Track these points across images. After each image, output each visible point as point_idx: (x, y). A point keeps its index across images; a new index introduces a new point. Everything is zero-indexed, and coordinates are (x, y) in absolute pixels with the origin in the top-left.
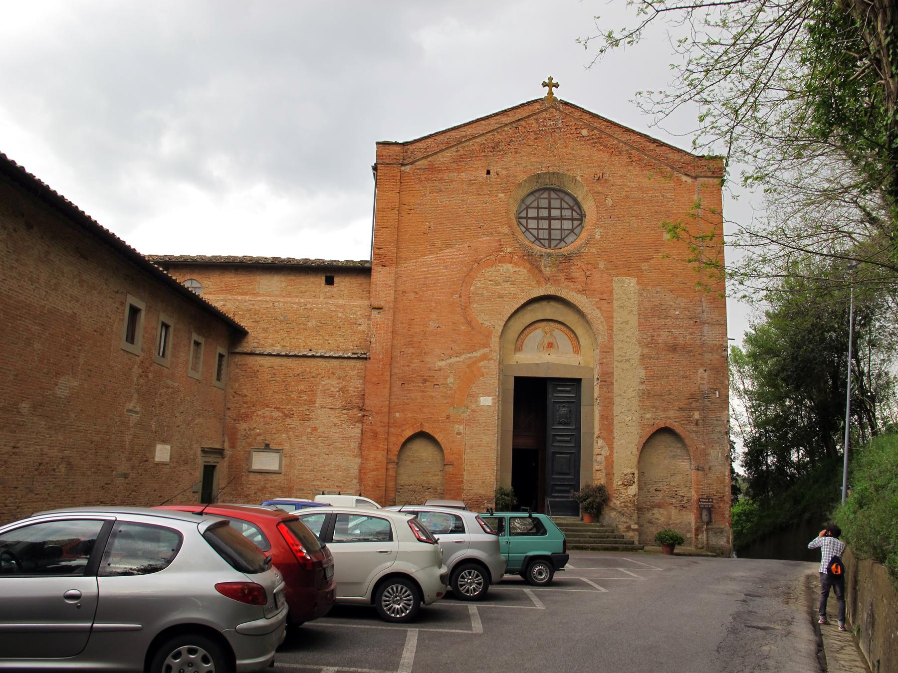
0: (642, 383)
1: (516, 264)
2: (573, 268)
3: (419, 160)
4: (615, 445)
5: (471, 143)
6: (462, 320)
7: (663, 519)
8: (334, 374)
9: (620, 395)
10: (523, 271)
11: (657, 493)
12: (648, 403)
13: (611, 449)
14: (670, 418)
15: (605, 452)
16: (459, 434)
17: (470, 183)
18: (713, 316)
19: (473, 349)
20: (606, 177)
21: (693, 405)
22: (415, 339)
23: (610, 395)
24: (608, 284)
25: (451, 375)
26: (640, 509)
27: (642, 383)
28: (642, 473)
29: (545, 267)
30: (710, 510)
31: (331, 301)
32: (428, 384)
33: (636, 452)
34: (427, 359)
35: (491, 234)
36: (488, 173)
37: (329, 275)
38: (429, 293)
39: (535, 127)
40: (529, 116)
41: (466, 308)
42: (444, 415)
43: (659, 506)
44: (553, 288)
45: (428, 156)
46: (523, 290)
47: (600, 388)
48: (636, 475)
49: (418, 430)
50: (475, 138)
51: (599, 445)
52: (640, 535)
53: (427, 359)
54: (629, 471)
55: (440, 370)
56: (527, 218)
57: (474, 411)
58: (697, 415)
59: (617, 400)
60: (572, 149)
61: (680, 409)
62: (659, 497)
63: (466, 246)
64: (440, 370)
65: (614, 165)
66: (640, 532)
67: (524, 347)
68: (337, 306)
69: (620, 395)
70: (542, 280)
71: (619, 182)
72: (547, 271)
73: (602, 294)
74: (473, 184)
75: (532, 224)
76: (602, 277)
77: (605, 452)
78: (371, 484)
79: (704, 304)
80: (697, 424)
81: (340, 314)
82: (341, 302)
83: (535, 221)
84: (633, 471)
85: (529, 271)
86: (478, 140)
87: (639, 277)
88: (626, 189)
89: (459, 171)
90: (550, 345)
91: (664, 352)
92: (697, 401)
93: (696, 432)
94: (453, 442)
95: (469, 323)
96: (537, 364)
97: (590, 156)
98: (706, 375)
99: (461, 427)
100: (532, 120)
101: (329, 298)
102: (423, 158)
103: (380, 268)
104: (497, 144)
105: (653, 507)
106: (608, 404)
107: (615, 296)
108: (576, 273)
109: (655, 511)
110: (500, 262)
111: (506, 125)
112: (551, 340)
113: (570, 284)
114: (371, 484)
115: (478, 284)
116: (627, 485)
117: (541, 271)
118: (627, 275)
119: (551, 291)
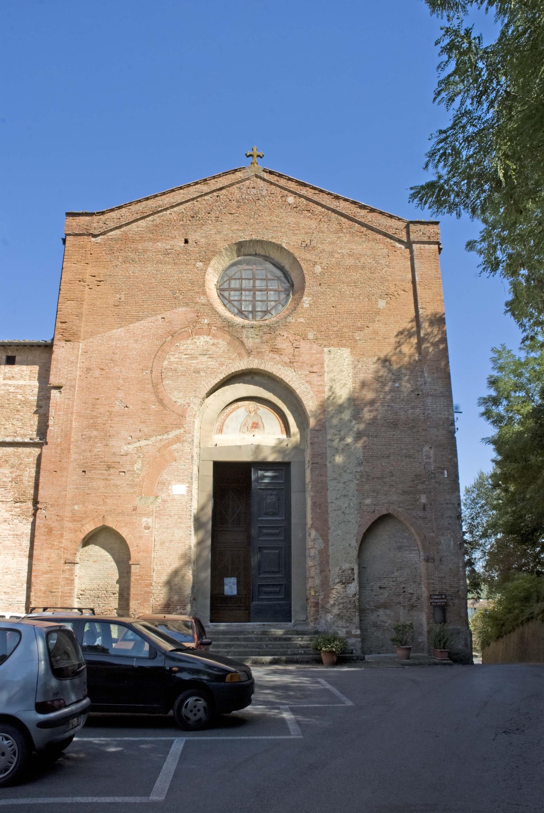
0: (360, 464)
1: (214, 336)
2: (279, 339)
3: (111, 230)
4: (330, 537)
5: (168, 212)
6: (153, 398)
7: (389, 622)
8: (7, 461)
9: (335, 479)
10: (222, 343)
11: (382, 591)
12: (367, 487)
13: (326, 541)
14: (391, 500)
15: (320, 544)
16: (147, 528)
17: (166, 253)
18: (435, 387)
19: (166, 430)
20: (314, 244)
21: (420, 487)
22: (100, 421)
23: (323, 478)
24: (318, 356)
25: (140, 461)
26: (362, 611)
27: (360, 464)
28: (362, 568)
29: (248, 337)
30: (443, 609)
31: (10, 382)
32: (112, 471)
33: (355, 544)
34: (112, 442)
35: (187, 305)
36: (186, 241)
37: (10, 354)
38: (117, 369)
39: (237, 195)
40: (232, 185)
41: (157, 384)
42: (130, 506)
43: (385, 606)
44: (256, 361)
45: (120, 227)
46: (222, 364)
47: (312, 471)
48: (356, 571)
49: (99, 525)
50: (172, 207)
51: (313, 541)
52: (363, 641)
53: (112, 442)
54: (346, 566)
55: (126, 455)
56: (230, 289)
57: (164, 501)
58: (423, 499)
59: (331, 484)
60: (277, 216)
61: (404, 492)
62: (384, 596)
63: (159, 317)
64: (126, 455)
65: (323, 232)
66: (363, 638)
67: (224, 429)
68: (18, 387)
69: (335, 479)
70: (243, 352)
71: (328, 248)
72: (249, 343)
73: (312, 367)
74: (168, 254)
75: (234, 296)
76: (311, 348)
77: (320, 544)
78: (43, 588)
79: (426, 375)
80: (424, 508)
81: (19, 397)
82: (21, 382)
83: (237, 293)
84: (351, 565)
85: (229, 344)
86: (175, 209)
87: (353, 348)
88: (336, 256)
89: (155, 241)
90: (255, 426)
91: (383, 429)
92: (423, 483)
93: (424, 518)
94: (141, 537)
95: (161, 401)
96: (240, 447)
97: (297, 224)
98: (432, 452)
99: (150, 520)
100: (234, 189)
101: (9, 379)
102: (116, 228)
103: (63, 343)
104: (197, 213)
105: (378, 607)
106: (321, 489)
107: (326, 369)
108: (283, 344)
109: (381, 612)
110: (196, 334)
111: (207, 194)
112: (255, 420)
113: (276, 356)
114: (43, 588)
115: (172, 359)
116: (345, 583)
117: (242, 343)
118: (340, 345)
119: (254, 363)
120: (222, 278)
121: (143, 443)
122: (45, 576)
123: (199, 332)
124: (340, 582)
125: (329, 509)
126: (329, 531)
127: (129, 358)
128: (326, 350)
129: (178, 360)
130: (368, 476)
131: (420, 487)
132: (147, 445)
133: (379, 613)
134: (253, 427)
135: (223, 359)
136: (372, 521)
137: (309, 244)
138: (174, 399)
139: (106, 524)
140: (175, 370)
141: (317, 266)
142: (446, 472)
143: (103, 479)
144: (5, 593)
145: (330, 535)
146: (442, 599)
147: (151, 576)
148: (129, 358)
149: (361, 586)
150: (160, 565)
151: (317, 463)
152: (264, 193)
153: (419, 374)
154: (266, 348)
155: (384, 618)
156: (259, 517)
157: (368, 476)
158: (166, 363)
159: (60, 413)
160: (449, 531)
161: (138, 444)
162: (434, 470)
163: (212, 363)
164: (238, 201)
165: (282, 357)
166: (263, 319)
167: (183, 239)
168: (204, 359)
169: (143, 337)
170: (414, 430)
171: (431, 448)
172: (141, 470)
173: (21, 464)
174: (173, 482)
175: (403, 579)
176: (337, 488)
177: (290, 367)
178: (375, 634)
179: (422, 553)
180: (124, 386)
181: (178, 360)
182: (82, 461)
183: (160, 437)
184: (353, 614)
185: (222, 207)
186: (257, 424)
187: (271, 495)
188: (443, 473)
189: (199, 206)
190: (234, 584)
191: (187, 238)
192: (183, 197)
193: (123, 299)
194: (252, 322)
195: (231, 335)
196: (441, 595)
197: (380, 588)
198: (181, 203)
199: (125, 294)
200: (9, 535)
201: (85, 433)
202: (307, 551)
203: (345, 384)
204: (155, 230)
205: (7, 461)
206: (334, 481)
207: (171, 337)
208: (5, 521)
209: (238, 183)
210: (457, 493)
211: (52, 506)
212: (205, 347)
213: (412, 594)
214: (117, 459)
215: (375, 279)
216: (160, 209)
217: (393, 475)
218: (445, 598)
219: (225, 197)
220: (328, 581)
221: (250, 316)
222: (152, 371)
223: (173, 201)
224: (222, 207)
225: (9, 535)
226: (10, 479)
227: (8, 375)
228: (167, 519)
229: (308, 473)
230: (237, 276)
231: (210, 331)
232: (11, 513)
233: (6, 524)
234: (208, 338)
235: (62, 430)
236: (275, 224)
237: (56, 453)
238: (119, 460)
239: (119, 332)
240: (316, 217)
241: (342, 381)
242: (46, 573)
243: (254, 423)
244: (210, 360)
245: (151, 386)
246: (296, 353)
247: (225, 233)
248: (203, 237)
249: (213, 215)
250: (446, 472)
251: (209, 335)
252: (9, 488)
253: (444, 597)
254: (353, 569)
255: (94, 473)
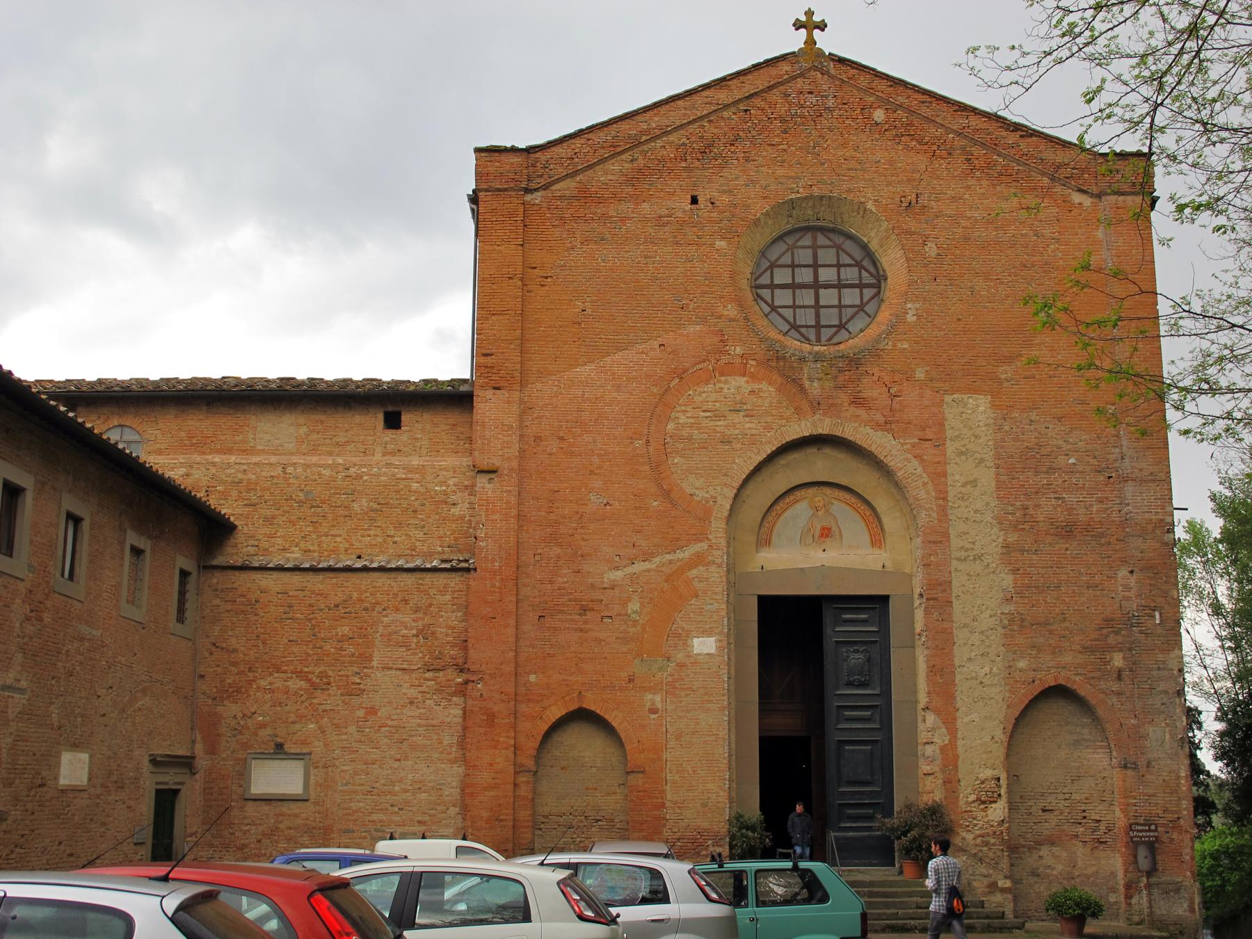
1: (753, 377)
2: (865, 380)
4: (959, 724)
7: (1060, 867)
8: (406, 601)
9: (966, 626)
13: (953, 732)
15: (941, 738)
16: (653, 711)
17: (660, 222)
19: (675, 544)
21: (1112, 640)
23: (946, 625)
26: (1013, 849)
27: (1008, 600)
28: (1014, 778)
31: (395, 460)
32: (589, 615)
35: (704, 320)
36: (694, 200)
37: (390, 409)
38: (587, 438)
42: (624, 675)
43: (1051, 841)
44: (827, 421)
45: (576, 173)
46: (768, 427)
47: (927, 612)
48: (1003, 782)
50: (666, 133)
52: (1016, 899)
54: (989, 773)
56: (772, 286)
57: (681, 666)
58: (1118, 661)
59: (960, 635)
60: (856, 148)
63: (656, 344)
65: (938, 178)
66: (1016, 894)
69: (966, 626)
70: (805, 406)
72: (814, 388)
74: (664, 225)
77: (941, 738)
79: (1125, 443)
80: (1119, 678)
81: (415, 486)
84: (996, 773)
85: (779, 390)
86: (672, 138)
88: (964, 223)
90: (826, 533)
91: (1049, 539)
93: (1119, 694)
94: (643, 727)
95: (666, 494)
96: (802, 570)
97: (891, 163)
98: (1132, 581)
99: (658, 698)
100: (775, 96)
101: (393, 454)
105: (1039, 843)
106: (943, 642)
107: (949, 433)
108: (870, 390)
109: (1045, 851)
110: (722, 374)
111: (726, 107)
113: (862, 412)
114: (485, 814)
116: (986, 801)
117: (802, 389)
119: (824, 426)
120: (758, 265)
121: (639, 567)
122: (487, 793)
123: (727, 370)
124: (978, 799)
125: (958, 677)
126: (958, 714)
127: (607, 418)
128: (948, 398)
129: (693, 421)
130: (1023, 620)
131: (1112, 640)
132: (648, 571)
133: (1041, 853)
134: (822, 535)
135: (769, 419)
136: (1031, 697)
137: (914, 201)
138: (689, 490)
139: (584, 706)
140: (690, 438)
141: (930, 244)
142: (1157, 614)
143: (576, 630)
144: (419, 822)
145: (959, 721)
146: (1150, 830)
147: (663, 791)
148: (607, 418)
149: (1012, 807)
150: (678, 772)
151: (936, 599)
152: (831, 102)
153: (1112, 440)
154: (843, 398)
155: (1049, 861)
156: (837, 689)
157: (1023, 620)
158: (670, 426)
159: (495, 517)
160: (1162, 717)
161: (629, 570)
162: (1137, 610)
163: (751, 425)
164: (783, 121)
165: (872, 412)
166: (835, 340)
167: (689, 197)
168: (738, 418)
169: (628, 379)
170: (1103, 541)
171: (1132, 572)
172: (640, 614)
173: (431, 605)
174: (694, 634)
175: (1083, 796)
176: (970, 642)
177: (887, 430)
178: (1036, 887)
179: (1114, 753)
180: (601, 468)
181: (693, 421)
182: (538, 600)
183: (668, 557)
184: (999, 853)
185: (754, 133)
186: (829, 529)
187: (856, 651)
188: (1154, 617)
189: (715, 131)
190: (1056, 679)
191: (696, 193)
192: (685, 115)
193: (589, 311)
194: (816, 348)
195: (784, 375)
196: (1149, 825)
197: (1044, 811)
198: (681, 126)
199: (592, 302)
200: (419, 726)
201: (540, 551)
202: (920, 747)
203: (982, 460)
204: (636, 178)
205: (406, 601)
206: (965, 630)
207: (677, 380)
208: (411, 703)
209: (782, 83)
210: (1176, 651)
211: (492, 676)
212: (738, 398)
213: (1098, 821)
214: (596, 595)
215: (1033, 266)
216: (644, 138)
217: (1064, 620)
218: (1156, 830)
219: (759, 112)
220: (957, 798)
221: (812, 334)
222: (648, 442)
223: (667, 122)
224: (754, 133)
225: (419, 726)
226: (414, 632)
227: (391, 447)
228: (687, 695)
229: (919, 615)
230: (786, 259)
231: (745, 367)
232: (420, 689)
233: (413, 708)
234: (742, 381)
235: (500, 547)
236: (852, 164)
237: (493, 586)
238: (602, 597)
239: (586, 371)
240: (926, 147)
241: (977, 455)
242: (489, 788)
243: (823, 529)
244: (747, 419)
245: (646, 468)
246: (896, 406)
247: (763, 183)
248: (725, 192)
249: (739, 147)
250: (1157, 614)
251: (744, 375)
252: (413, 646)
253: (1153, 827)
254: (998, 779)
255: (560, 620)
